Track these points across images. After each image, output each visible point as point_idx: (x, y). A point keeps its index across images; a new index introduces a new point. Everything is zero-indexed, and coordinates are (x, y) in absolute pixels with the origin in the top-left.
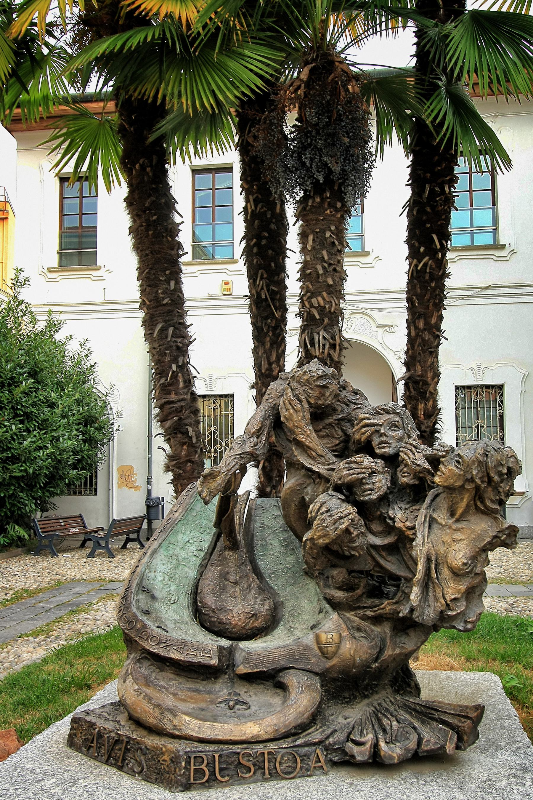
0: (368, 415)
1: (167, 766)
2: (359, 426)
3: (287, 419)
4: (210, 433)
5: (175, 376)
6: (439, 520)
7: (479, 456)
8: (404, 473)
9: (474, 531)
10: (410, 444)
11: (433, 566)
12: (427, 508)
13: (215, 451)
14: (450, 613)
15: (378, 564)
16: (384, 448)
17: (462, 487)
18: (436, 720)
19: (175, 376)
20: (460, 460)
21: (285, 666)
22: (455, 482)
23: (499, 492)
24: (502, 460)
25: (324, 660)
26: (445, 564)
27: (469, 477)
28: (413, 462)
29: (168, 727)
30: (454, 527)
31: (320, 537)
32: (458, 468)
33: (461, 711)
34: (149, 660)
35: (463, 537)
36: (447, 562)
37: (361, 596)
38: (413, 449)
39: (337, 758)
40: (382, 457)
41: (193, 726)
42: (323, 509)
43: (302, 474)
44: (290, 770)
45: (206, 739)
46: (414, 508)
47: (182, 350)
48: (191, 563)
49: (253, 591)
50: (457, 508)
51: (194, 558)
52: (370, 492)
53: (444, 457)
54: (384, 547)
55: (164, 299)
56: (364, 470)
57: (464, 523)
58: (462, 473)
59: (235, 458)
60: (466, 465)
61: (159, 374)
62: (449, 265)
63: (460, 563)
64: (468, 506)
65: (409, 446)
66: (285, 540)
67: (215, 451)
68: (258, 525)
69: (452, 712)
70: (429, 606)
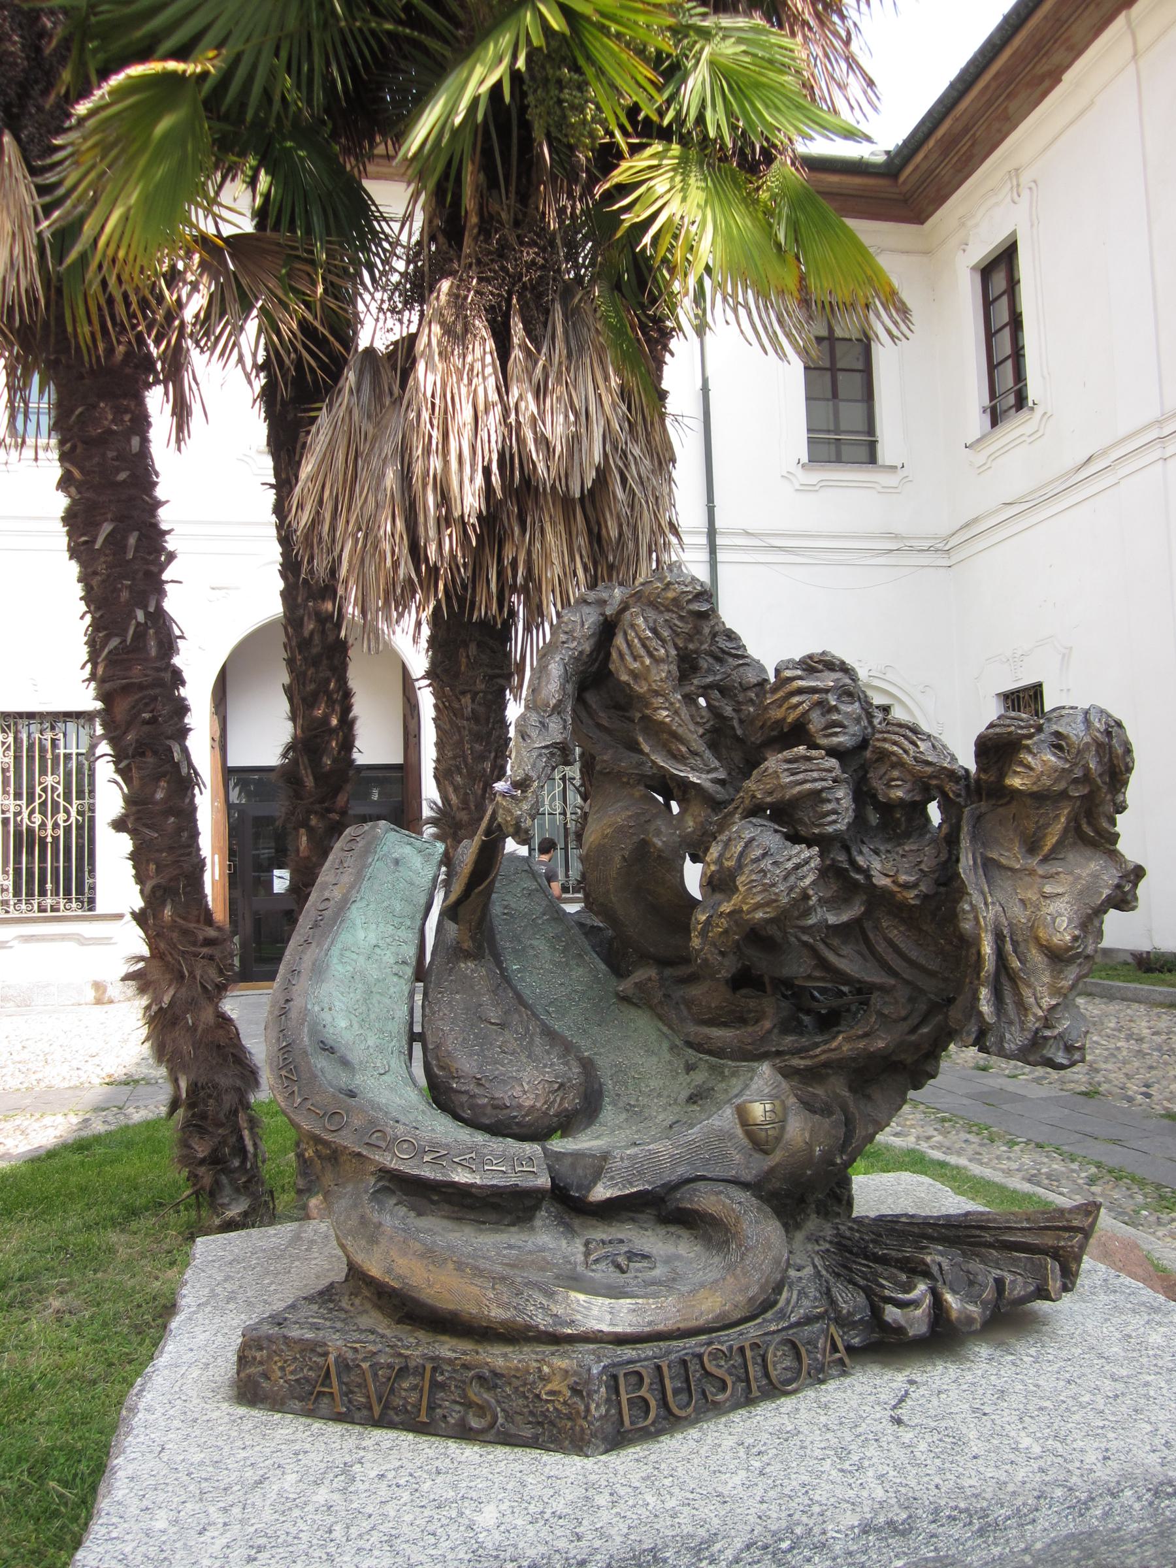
0: (799, 672)
1: (565, 1403)
4: (44, 790)
5: (140, 635)
9: (1079, 877)
11: (1009, 947)
13: (56, 826)
14: (1048, 1033)
15: (824, 964)
16: (836, 734)
18: (990, 1246)
19: (140, 635)
21: (686, 1175)
25: (757, 1156)
27: (1078, 773)
28: (915, 758)
29: (542, 1321)
30: (1040, 872)
31: (758, 906)
33: (1048, 1220)
34: (393, 1192)
35: (1060, 891)
36: (1037, 939)
37: (770, 1032)
38: (910, 734)
39: (857, 1340)
41: (598, 1313)
43: (637, 794)
44: (789, 1375)
45: (631, 1334)
47: (151, 585)
49: (537, 1040)
50: (1045, 836)
51: (395, 979)
52: (834, 817)
53: (1030, 736)
54: (836, 929)
55: (118, 470)
61: (105, 629)
63: (1068, 938)
66: (557, 937)
67: (56, 826)
69: (1025, 1225)
70: (1011, 1023)
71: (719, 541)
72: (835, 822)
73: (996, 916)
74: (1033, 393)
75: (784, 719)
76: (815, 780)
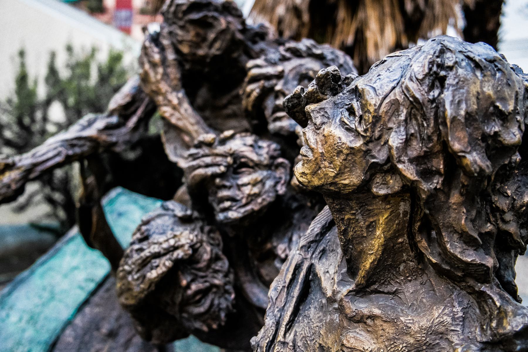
7: (413, 86)
9: (406, 331)
12: (307, 247)
17: (364, 187)
20: (356, 105)
22: (340, 173)
23: (496, 210)
24: (503, 99)
27: (381, 156)
32: (349, 130)
56: (219, 159)
57: (382, 300)
58: (358, 143)
60: (369, 117)
64: (389, 249)
76: (207, 166)
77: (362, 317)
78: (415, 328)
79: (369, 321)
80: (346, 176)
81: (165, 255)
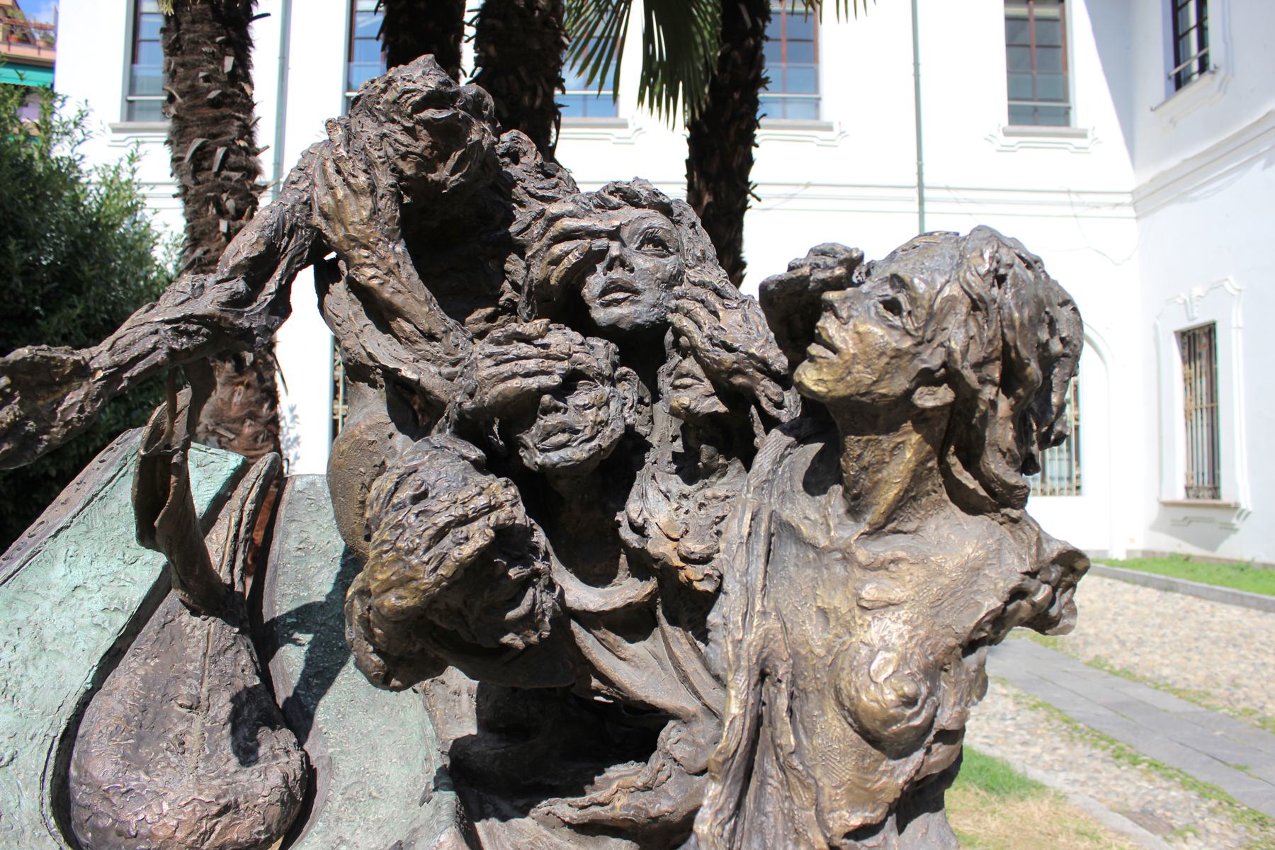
2: (545, 240)
3: (325, 216)
6: (805, 530)
8: (682, 376)
10: (703, 285)
12: (759, 488)
16: (617, 302)
20: (902, 298)
26: (830, 694)
27: (932, 359)
31: (388, 587)
36: (838, 691)
38: (712, 298)
40: (610, 332)
42: (405, 493)
46: (709, 493)
48: (82, 645)
51: (94, 632)
52: (562, 437)
58: (907, 343)
59: (156, 332)
60: (922, 313)
62: (767, 64)
63: (891, 696)
64: (917, 477)
65: (698, 291)
68: (292, 544)
71: (926, 194)
72: (564, 445)
73: (766, 638)
74: (1213, 60)
75: (547, 280)
76: (528, 375)
77: (882, 563)
78: (949, 565)
79: (892, 567)
80: (883, 384)
81: (474, 519)
